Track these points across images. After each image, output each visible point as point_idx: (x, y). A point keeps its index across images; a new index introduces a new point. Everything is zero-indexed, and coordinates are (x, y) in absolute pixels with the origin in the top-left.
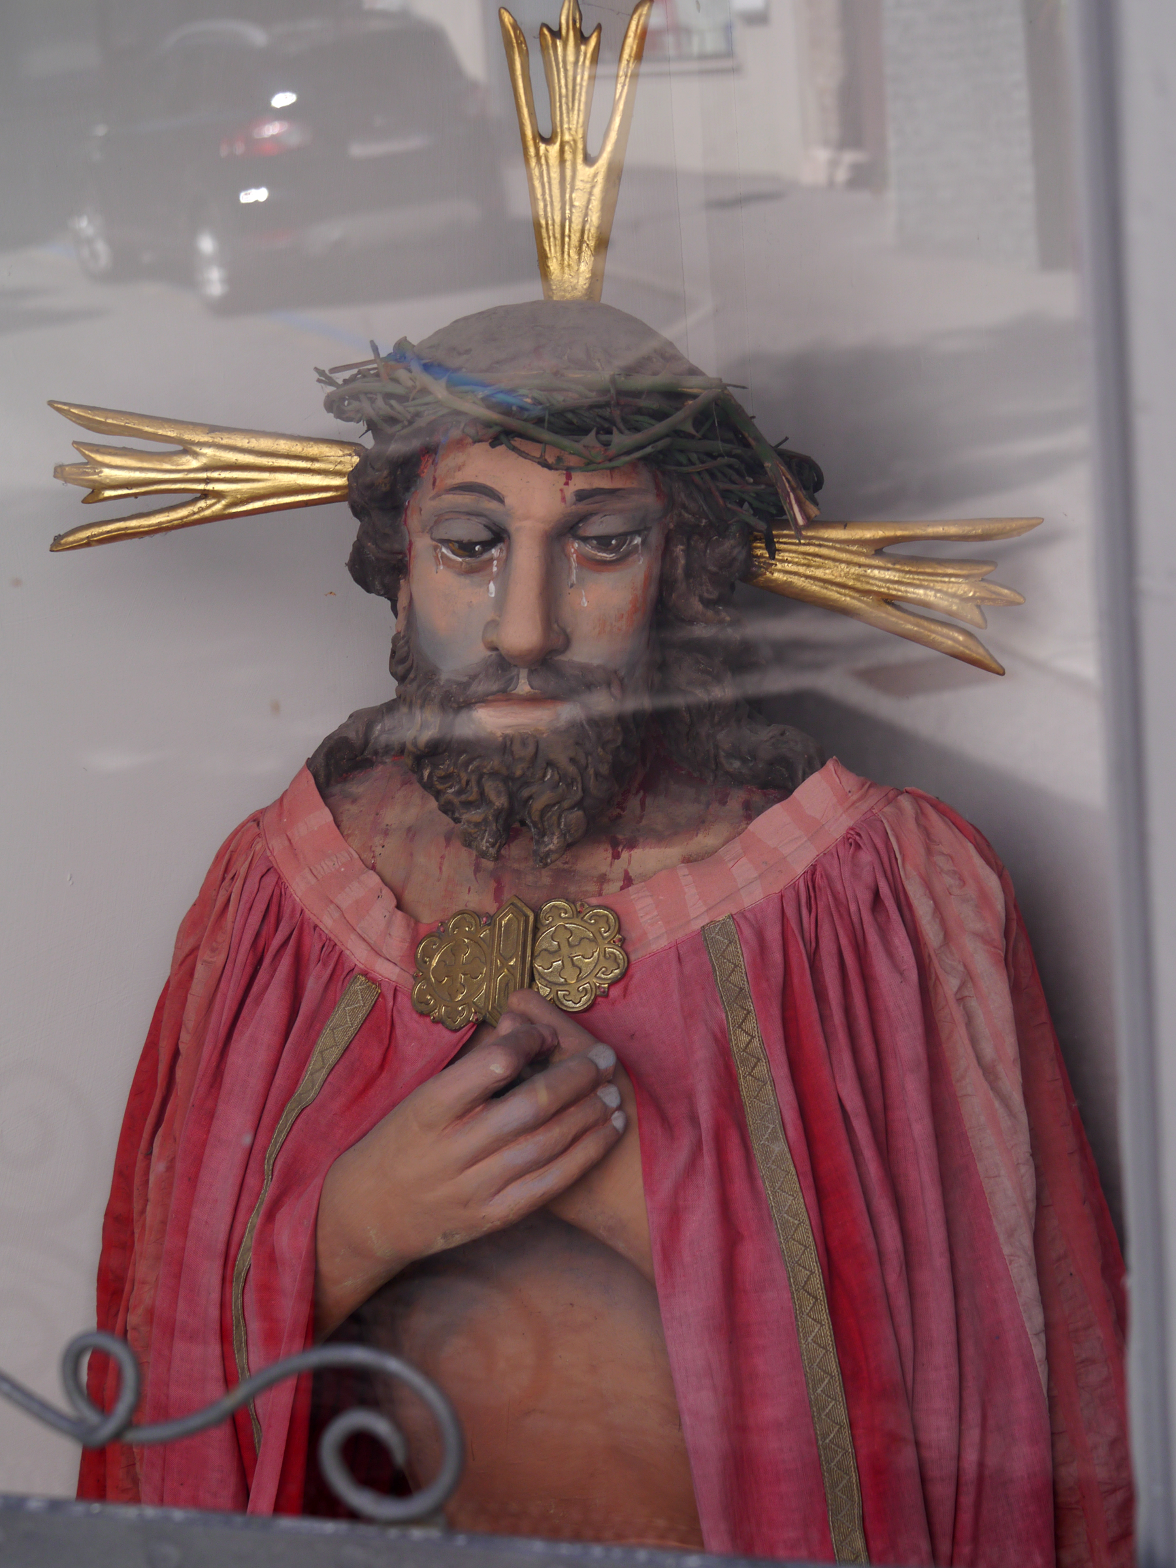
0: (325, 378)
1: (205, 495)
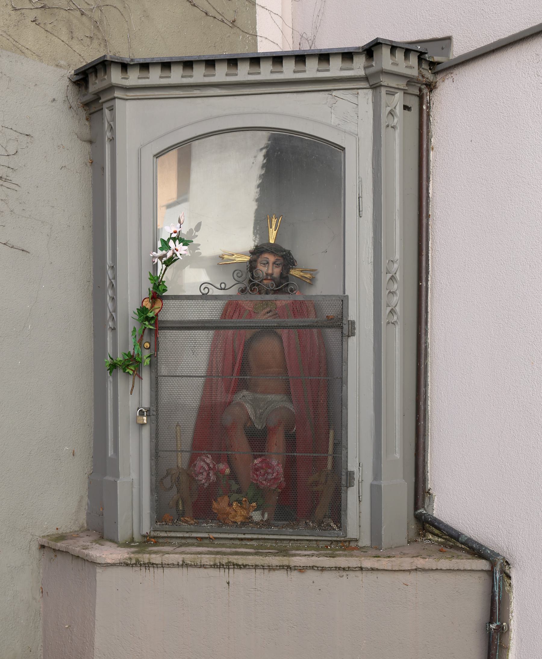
1: (234, 260)
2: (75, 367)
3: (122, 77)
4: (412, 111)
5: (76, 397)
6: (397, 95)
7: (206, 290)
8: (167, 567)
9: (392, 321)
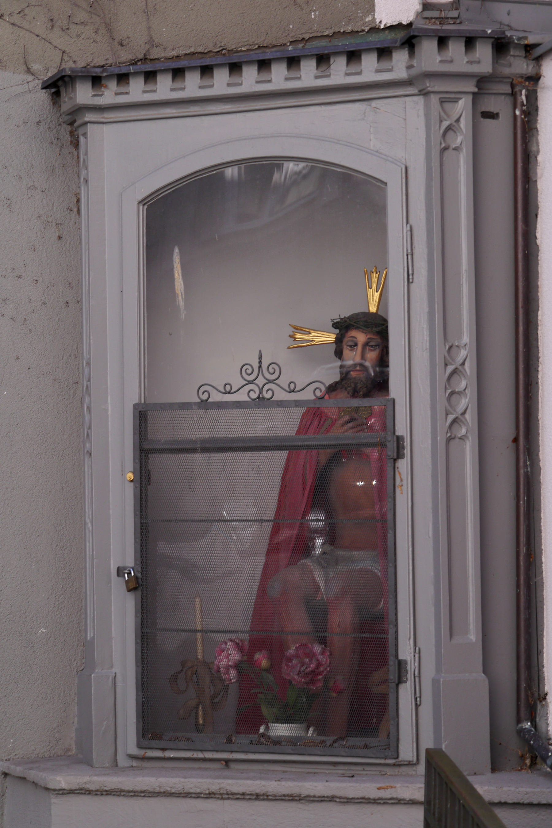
0: (332, 320)
2: (54, 510)
3: (93, 93)
4: (500, 119)
5: (56, 555)
6: (461, 103)
7: (206, 395)
8: (141, 796)
9: (459, 436)
